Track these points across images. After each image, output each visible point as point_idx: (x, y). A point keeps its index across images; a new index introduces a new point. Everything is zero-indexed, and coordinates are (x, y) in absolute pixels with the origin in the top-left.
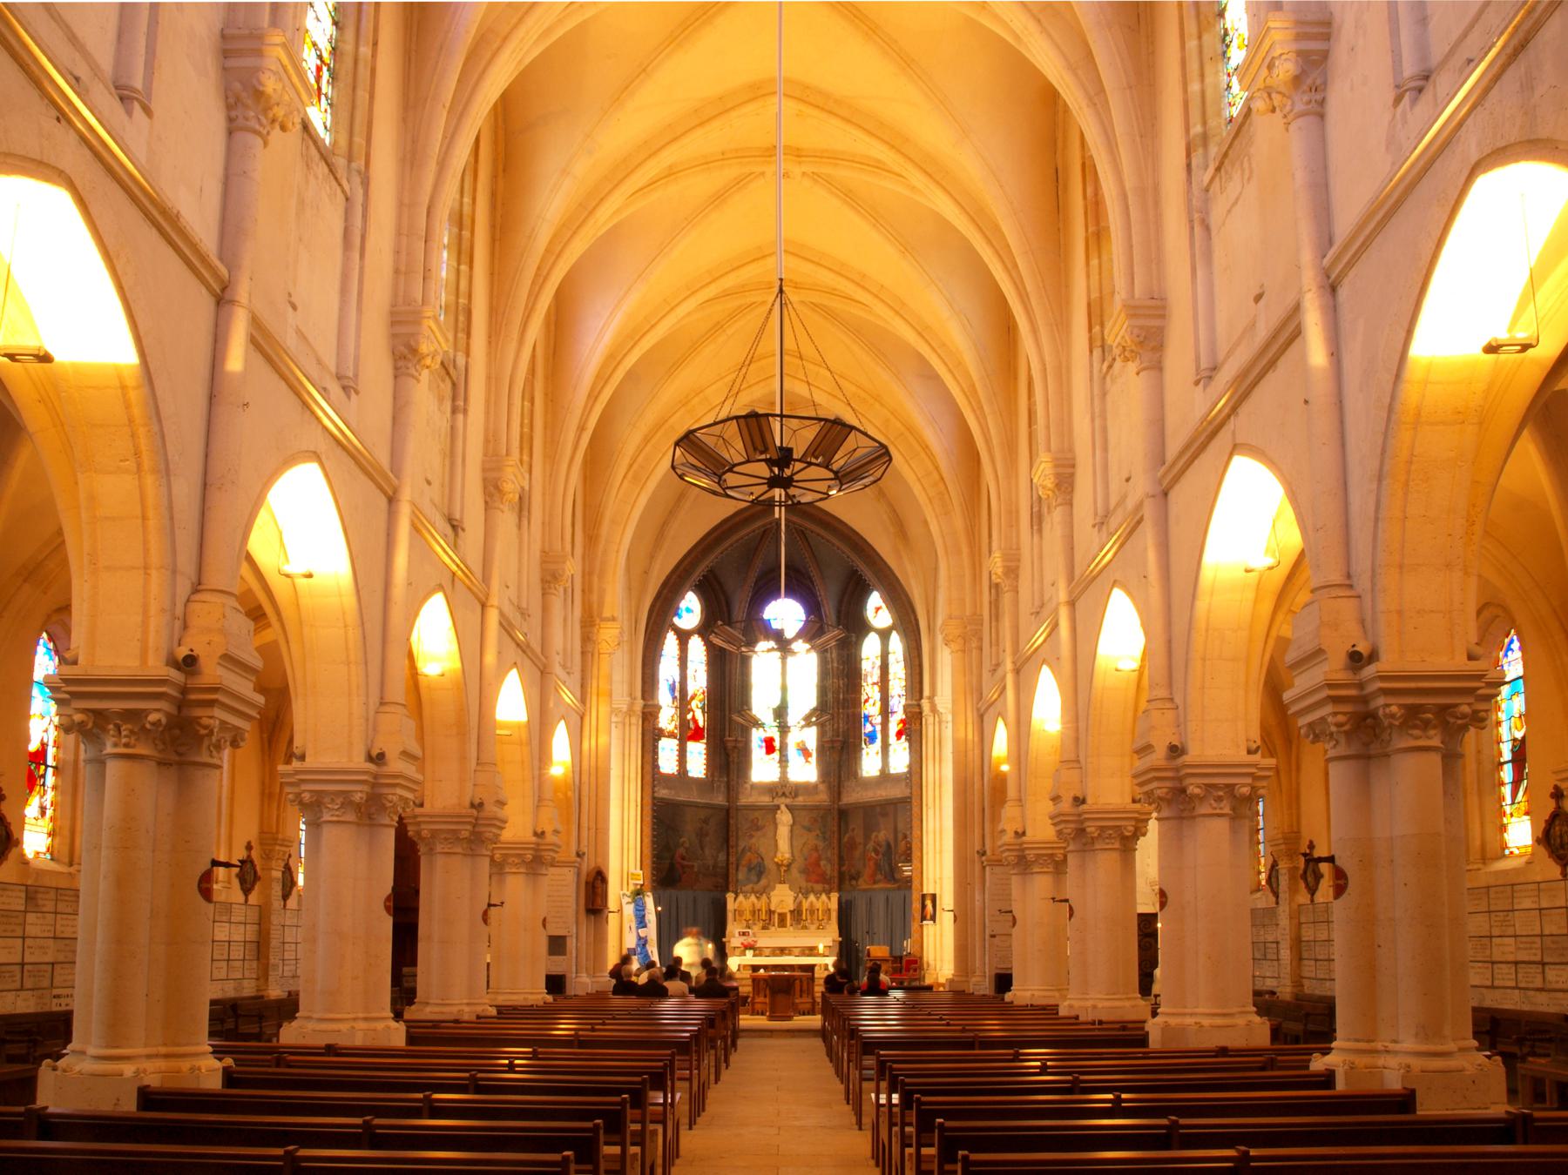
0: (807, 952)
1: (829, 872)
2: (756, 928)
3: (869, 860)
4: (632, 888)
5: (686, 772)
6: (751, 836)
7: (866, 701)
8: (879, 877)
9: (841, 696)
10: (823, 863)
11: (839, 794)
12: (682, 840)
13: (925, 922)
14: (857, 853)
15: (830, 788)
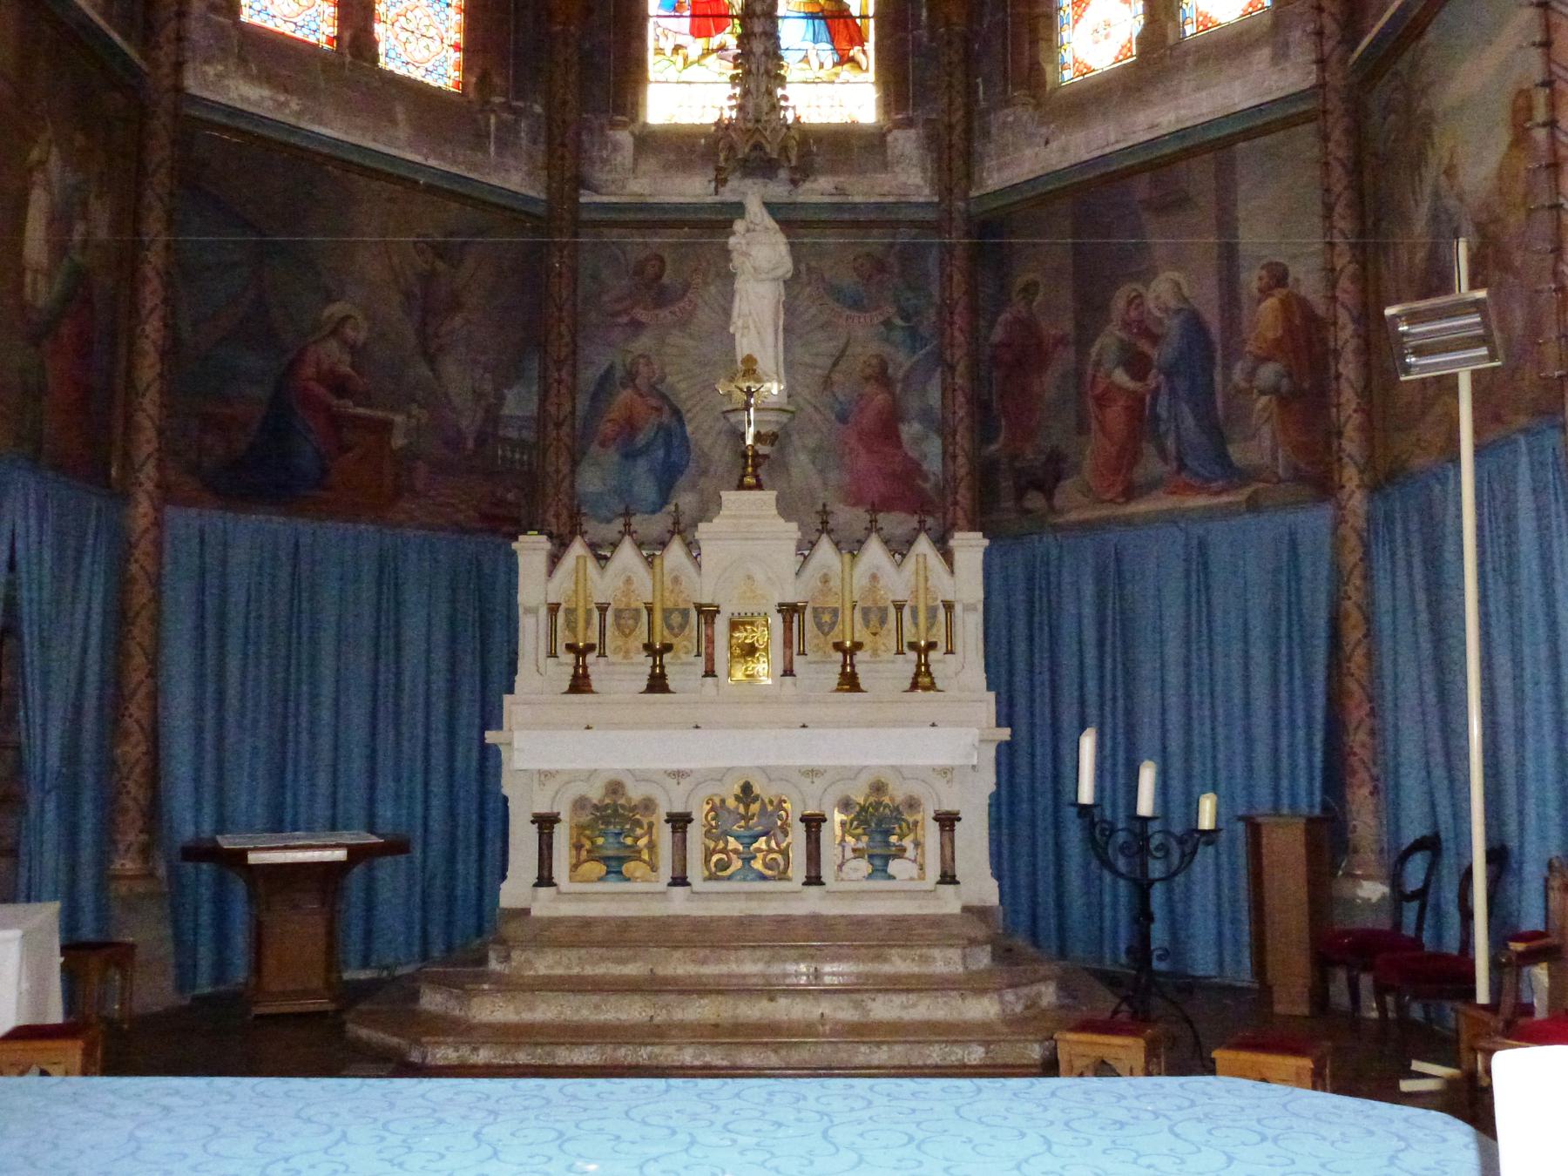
1: (933, 464)
6: (637, 326)
8: (1151, 465)
10: (910, 430)
11: (969, 157)
12: (336, 309)
14: (1049, 384)
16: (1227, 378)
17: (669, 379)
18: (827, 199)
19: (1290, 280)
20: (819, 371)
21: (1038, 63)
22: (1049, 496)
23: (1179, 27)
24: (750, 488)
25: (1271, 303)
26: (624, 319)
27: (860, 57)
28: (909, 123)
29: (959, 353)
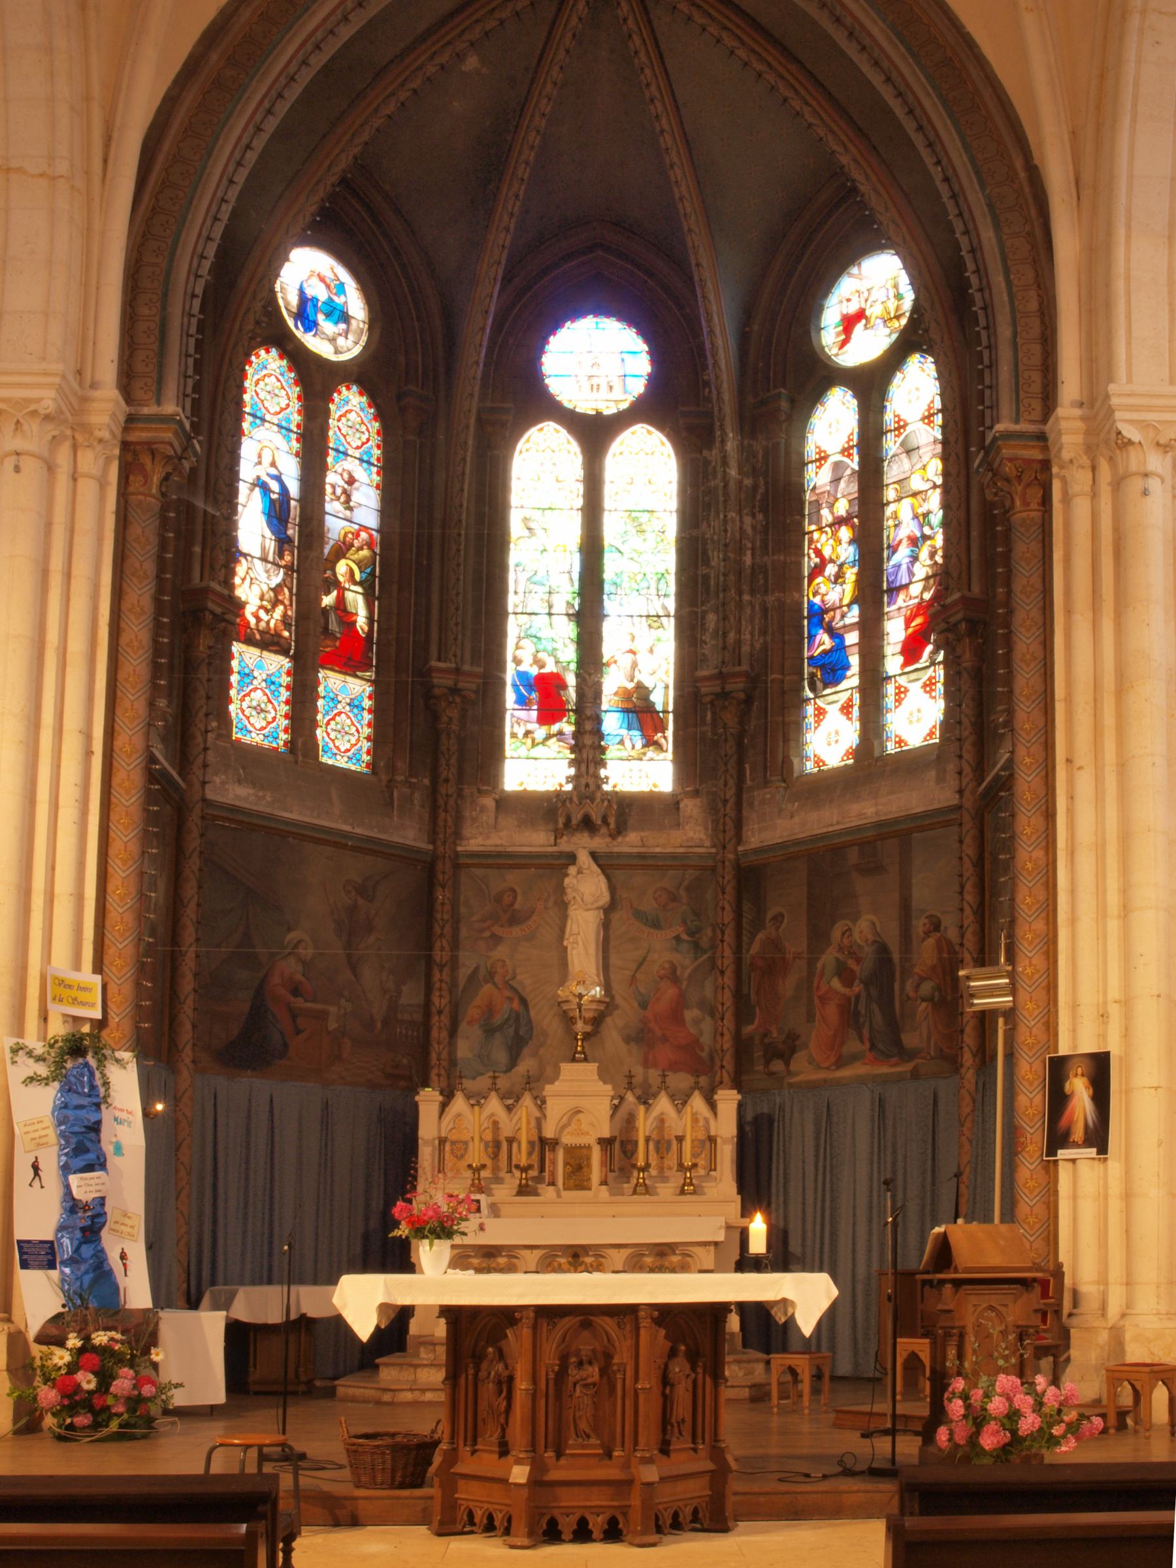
0: (648, 1260)
1: (706, 1039)
2: (504, 1192)
3: (824, 999)
4: (57, 1028)
5: (311, 747)
6: (496, 939)
7: (818, 570)
9: (748, 559)
10: (690, 1014)
11: (739, 824)
12: (293, 936)
13: (1062, 1154)
14: (788, 986)
15: (714, 809)
16: (902, 989)
17: (518, 978)
18: (636, 850)
19: (942, 928)
20: (628, 972)
21: (788, 756)
22: (787, 1064)
23: (883, 748)
24: (579, 1061)
25: (931, 941)
26: (487, 934)
27: (663, 741)
28: (696, 793)
29: (726, 962)
